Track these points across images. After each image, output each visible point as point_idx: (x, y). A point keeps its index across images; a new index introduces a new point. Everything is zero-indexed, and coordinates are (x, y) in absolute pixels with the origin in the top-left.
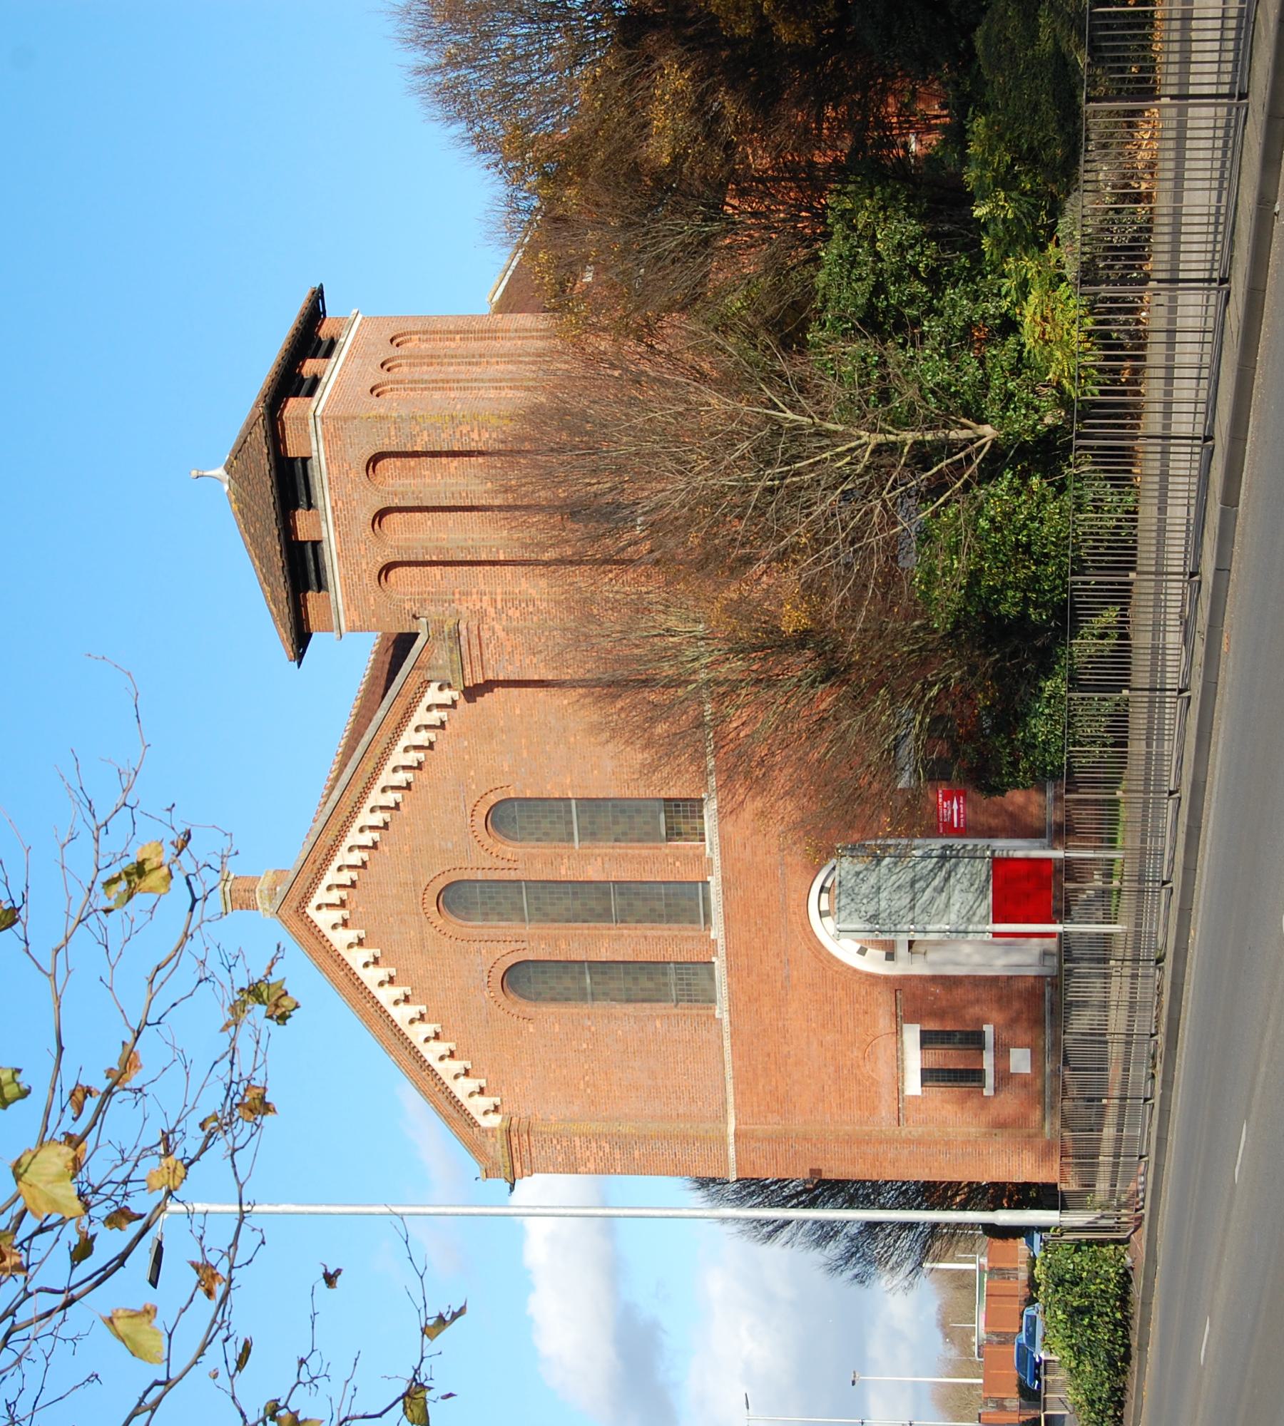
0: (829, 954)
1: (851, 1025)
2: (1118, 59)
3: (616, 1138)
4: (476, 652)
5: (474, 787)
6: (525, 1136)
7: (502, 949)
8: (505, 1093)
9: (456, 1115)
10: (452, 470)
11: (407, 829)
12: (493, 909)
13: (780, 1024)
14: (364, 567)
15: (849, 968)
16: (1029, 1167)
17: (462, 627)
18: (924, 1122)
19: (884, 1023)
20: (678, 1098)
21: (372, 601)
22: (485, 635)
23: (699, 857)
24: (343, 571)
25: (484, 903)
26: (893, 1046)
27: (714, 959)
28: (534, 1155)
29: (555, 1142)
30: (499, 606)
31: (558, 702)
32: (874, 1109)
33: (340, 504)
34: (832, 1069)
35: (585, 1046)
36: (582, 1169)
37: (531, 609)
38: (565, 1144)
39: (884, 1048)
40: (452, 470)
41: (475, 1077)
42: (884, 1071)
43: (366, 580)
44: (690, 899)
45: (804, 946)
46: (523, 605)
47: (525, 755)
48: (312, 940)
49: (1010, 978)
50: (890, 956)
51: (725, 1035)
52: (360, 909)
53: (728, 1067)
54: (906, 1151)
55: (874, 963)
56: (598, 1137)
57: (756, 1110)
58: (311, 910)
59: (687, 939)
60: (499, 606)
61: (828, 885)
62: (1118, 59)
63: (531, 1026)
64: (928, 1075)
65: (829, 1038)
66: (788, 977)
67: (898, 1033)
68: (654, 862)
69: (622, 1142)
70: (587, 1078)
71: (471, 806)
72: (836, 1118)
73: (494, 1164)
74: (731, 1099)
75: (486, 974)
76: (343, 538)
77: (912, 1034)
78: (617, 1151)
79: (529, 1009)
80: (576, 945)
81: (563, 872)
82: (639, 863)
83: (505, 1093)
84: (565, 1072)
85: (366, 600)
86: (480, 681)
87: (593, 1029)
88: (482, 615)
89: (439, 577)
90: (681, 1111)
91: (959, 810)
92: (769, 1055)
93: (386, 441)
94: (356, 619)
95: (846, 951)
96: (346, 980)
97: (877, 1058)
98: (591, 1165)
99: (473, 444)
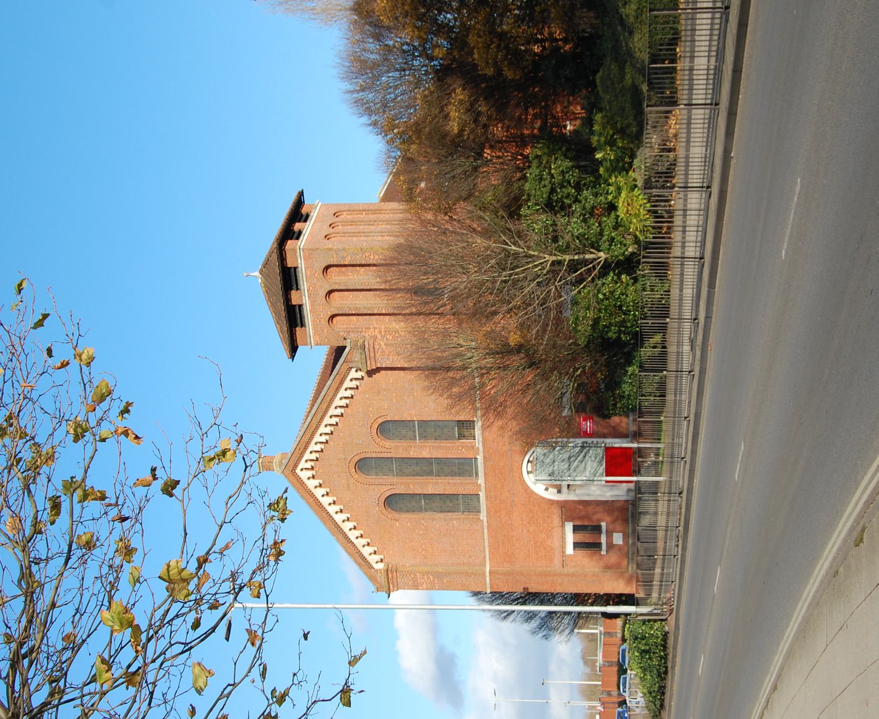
2: (660, 88)
4: (372, 355)
7: (385, 488)
17: (366, 343)
19: (556, 521)
22: (377, 347)
23: (473, 447)
39: (557, 533)
49: (613, 501)
53: (486, 541)
55: (551, 495)
56: (428, 573)
58: (298, 471)
62: (660, 88)
64: (577, 545)
67: (563, 526)
69: (438, 575)
74: (487, 556)
76: (313, 303)
77: (569, 527)
79: (397, 515)
86: (374, 367)
88: (375, 338)
95: (539, 489)
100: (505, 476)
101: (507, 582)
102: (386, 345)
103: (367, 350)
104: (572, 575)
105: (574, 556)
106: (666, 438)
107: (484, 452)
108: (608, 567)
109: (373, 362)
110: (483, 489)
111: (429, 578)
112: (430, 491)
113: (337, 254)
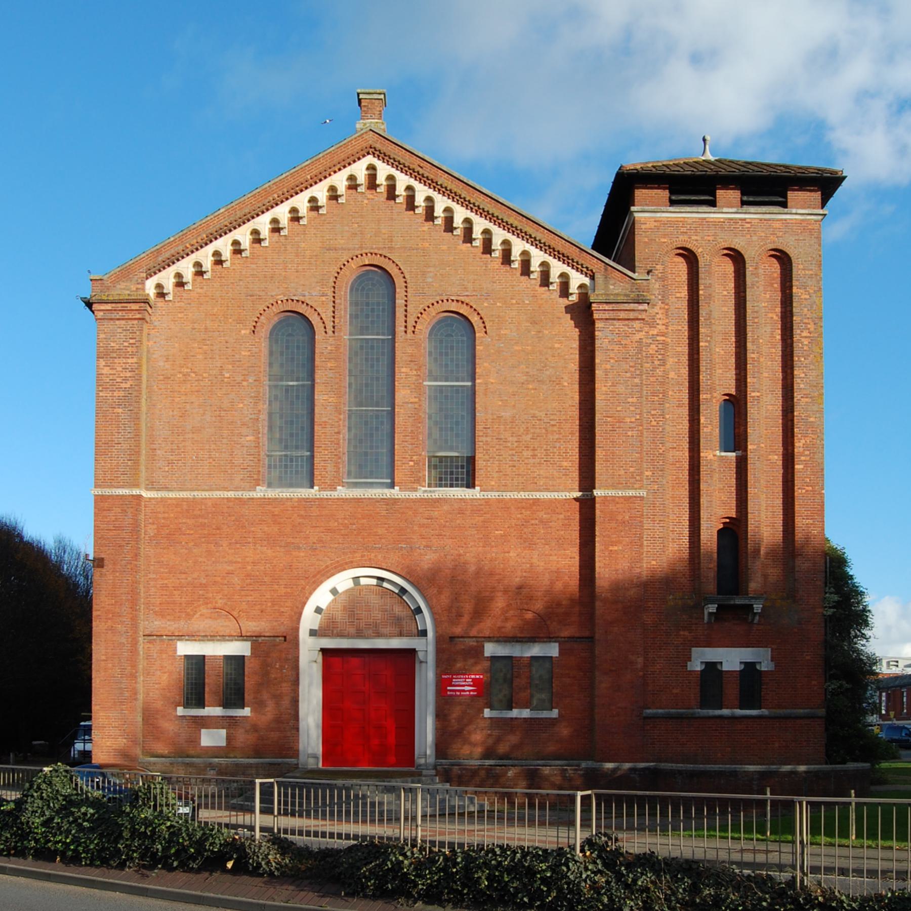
0: (322, 582)
1: (250, 598)
2: (340, 812)
3: (135, 394)
4: (622, 315)
5: (486, 304)
6: (138, 316)
7: (327, 315)
8: (177, 304)
9: (160, 259)
10: (770, 315)
11: (445, 247)
12: (362, 310)
13: (250, 540)
14: (694, 238)
15: (307, 599)
16: (108, 744)
17: (645, 306)
18: (148, 657)
19: (251, 626)
20: (172, 451)
21: (663, 240)
22: (637, 325)
23: (419, 481)
24: (690, 221)
25: (367, 304)
26: (227, 632)
27: (316, 488)
28: (117, 322)
29: (131, 341)
30: (658, 338)
31: (566, 378)
32: (161, 615)
33: (749, 225)
34: (204, 581)
35: (227, 375)
36: (102, 363)
37: (657, 363)
38: (129, 349)
39: (230, 626)
40: (770, 315)
41: (194, 280)
42: (199, 624)
43: (681, 237)
44: (371, 472)
45: (329, 562)
46: (660, 357)
47: (516, 348)
48: (343, 156)
49: (298, 729)
50: (313, 633)
51: (240, 493)
52: (366, 201)
53: (206, 494)
54: (124, 640)
55: (309, 620)
56: (138, 378)
57: (160, 516)
58: (370, 159)
59: (337, 465)
60: (658, 338)
61: (385, 585)
62: (340, 812)
63: (248, 332)
64: (197, 663)
65: (236, 580)
66: (299, 548)
67: (242, 637)
68: (415, 442)
69: (131, 399)
70: (193, 375)
71: (467, 301)
72: (152, 583)
73: (108, 288)
74: (172, 495)
75: (302, 298)
76: (719, 224)
77: (240, 648)
78: (122, 394)
79: (264, 332)
80: (331, 375)
81: (404, 370)
82: (412, 432)
83: (177, 304)
84: (200, 357)
85: (664, 236)
86: (596, 316)
87: (245, 383)
88: (653, 325)
89: (678, 295)
90: (158, 452)
91: (464, 691)
92: (218, 529)
93: (801, 267)
94: (647, 226)
95: (321, 597)
96: (302, 180)
97: (216, 619)
98: (106, 371)
99: (798, 332)
100: (355, 535)
101: (117, 528)
102: (640, 341)
103: (632, 306)
104: (134, 651)
105: (173, 655)
106: (773, 837)
107: (408, 500)
108: (149, 716)
109: (607, 315)
110: (326, 494)
111: (126, 379)
112: (320, 397)
113: (811, 277)
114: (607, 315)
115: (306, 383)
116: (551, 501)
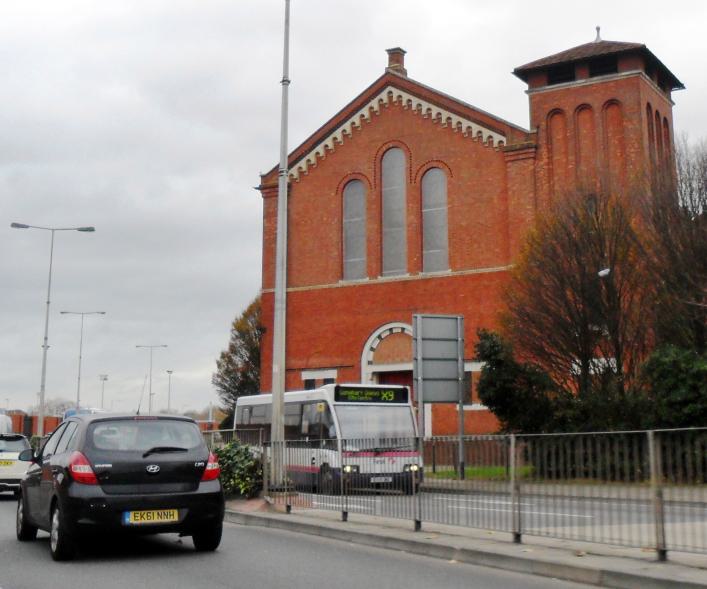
4: (521, 157)
39: (325, 361)
42: (314, 361)
76: (577, 91)
114: (512, 158)
115: (351, 260)
116: (490, 273)
